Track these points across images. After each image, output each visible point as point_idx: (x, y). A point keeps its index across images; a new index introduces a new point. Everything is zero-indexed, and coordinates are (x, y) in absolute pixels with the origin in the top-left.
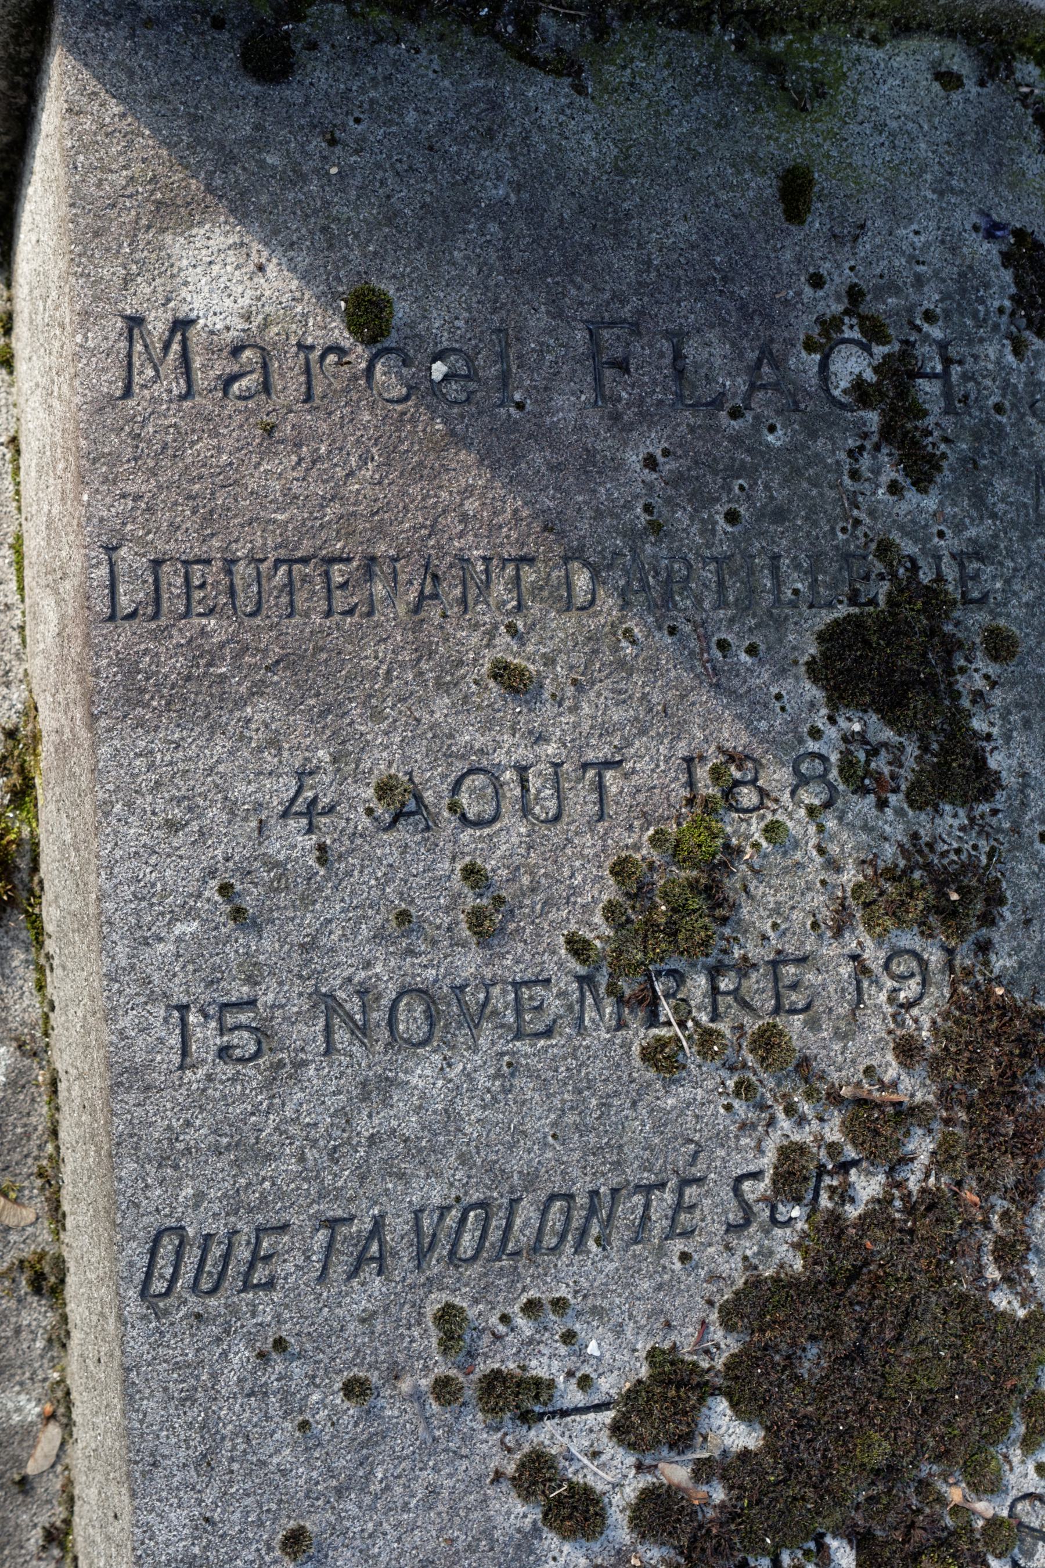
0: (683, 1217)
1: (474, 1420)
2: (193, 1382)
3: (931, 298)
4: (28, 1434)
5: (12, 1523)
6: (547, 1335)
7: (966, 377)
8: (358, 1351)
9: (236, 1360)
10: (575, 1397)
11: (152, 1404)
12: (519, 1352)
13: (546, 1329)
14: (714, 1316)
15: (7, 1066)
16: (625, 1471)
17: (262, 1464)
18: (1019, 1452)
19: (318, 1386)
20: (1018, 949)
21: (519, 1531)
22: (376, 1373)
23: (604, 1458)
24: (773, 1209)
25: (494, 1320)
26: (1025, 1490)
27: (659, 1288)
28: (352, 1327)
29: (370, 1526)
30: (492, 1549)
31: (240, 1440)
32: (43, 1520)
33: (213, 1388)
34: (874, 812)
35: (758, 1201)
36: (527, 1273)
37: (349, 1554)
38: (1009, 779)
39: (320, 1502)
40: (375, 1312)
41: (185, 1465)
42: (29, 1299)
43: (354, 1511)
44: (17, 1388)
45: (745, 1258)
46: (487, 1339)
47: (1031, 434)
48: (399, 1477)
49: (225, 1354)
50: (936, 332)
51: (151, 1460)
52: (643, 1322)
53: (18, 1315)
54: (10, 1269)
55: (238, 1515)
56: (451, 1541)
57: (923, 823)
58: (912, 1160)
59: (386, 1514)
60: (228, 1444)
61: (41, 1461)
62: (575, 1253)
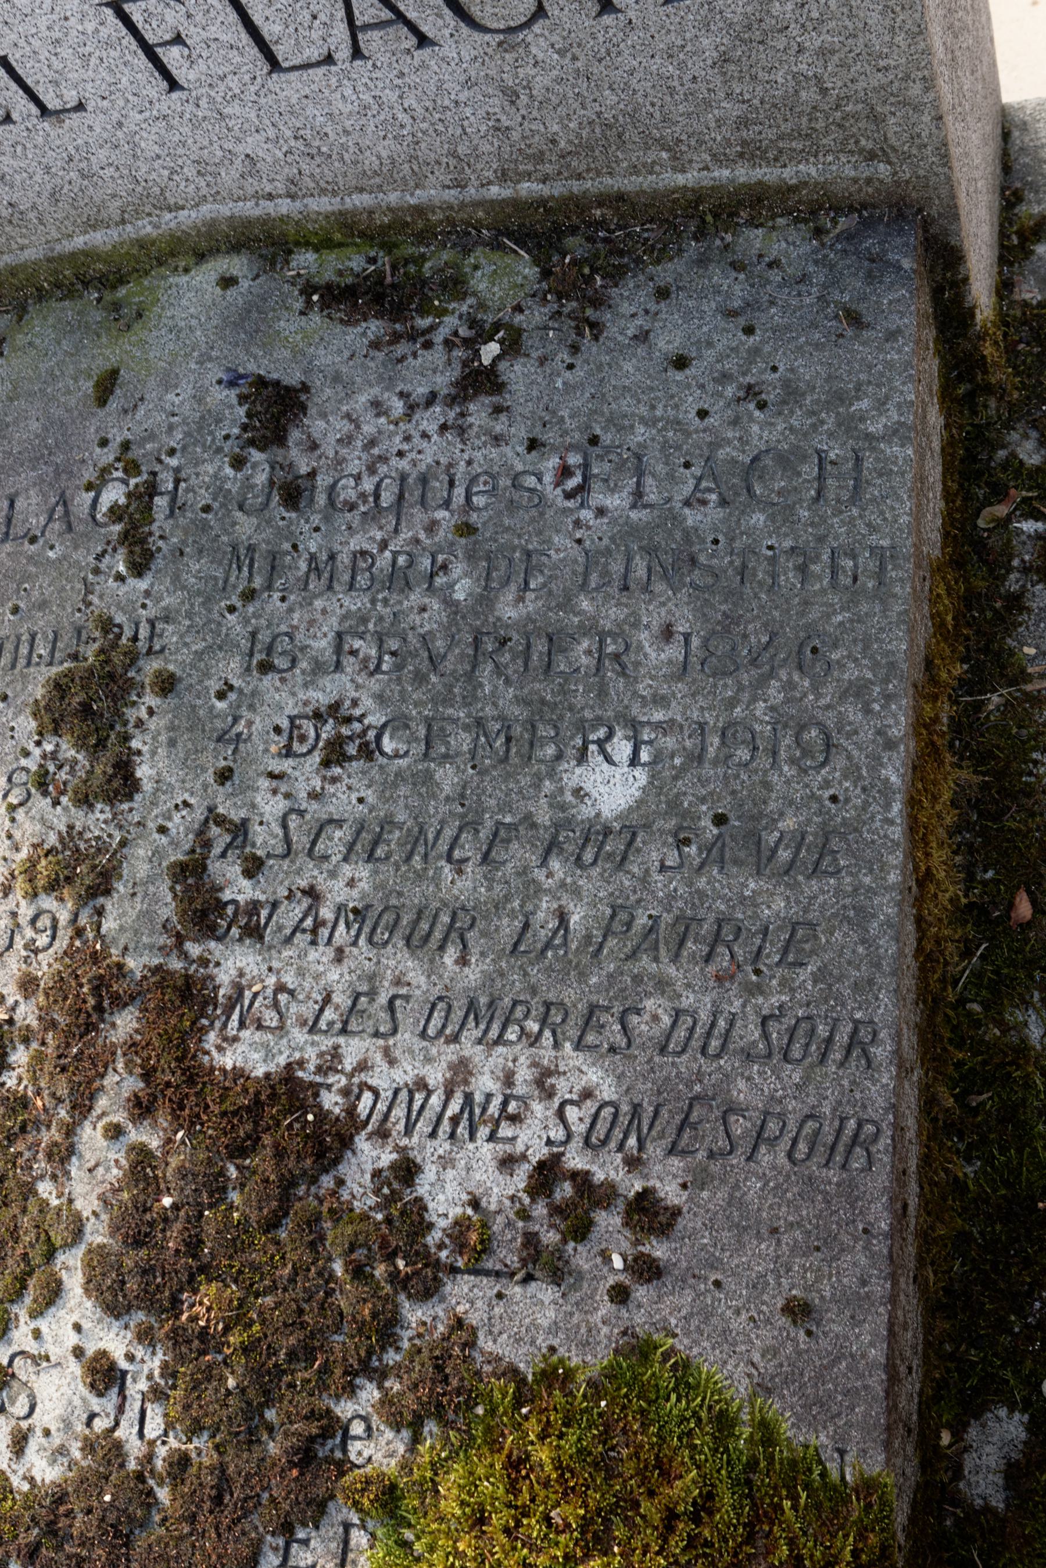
3: (176, 439)
7: (187, 490)
20: (120, 916)
34: (50, 809)
38: (147, 786)
47: (234, 524)
50: (174, 462)
57: (80, 818)
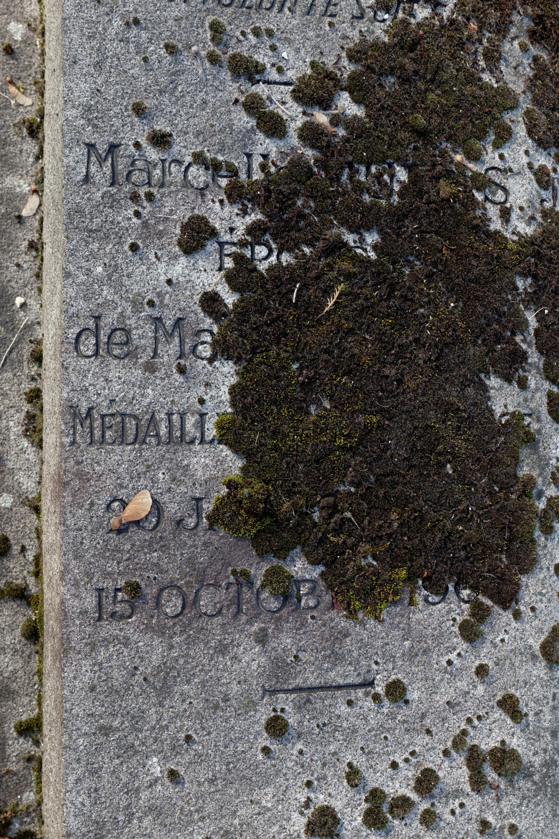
0: (331, 7)
1: (226, 75)
2: (95, 30)
4: (23, 198)
5: (14, 235)
6: (263, 45)
8: (173, 33)
9: (115, 24)
10: (274, 75)
11: (75, 36)
12: (249, 50)
13: (262, 43)
14: (344, 54)
15: (22, 34)
16: (297, 114)
17: (126, 72)
18: (491, 147)
19: (153, 44)
21: (245, 128)
22: (181, 44)
23: (287, 106)
24: (375, 14)
25: (238, 33)
26: (493, 165)
27: (318, 36)
28: (170, 22)
29: (174, 110)
30: (231, 133)
31: (115, 59)
32: (29, 237)
33: (104, 34)
35: (368, 7)
36: (254, 15)
37: (164, 120)
39: (151, 95)
40: (182, 18)
41: (89, 65)
42: (27, 139)
43: (167, 102)
44: (19, 177)
45: (361, 31)
46: (234, 40)
48: (188, 93)
49: (110, 20)
51: (74, 60)
52: (310, 50)
53: (22, 144)
54: (19, 123)
55: (112, 91)
56: (212, 126)
58: (445, 6)
59: (182, 107)
60: (109, 60)
61: (29, 211)
62: (279, 12)
